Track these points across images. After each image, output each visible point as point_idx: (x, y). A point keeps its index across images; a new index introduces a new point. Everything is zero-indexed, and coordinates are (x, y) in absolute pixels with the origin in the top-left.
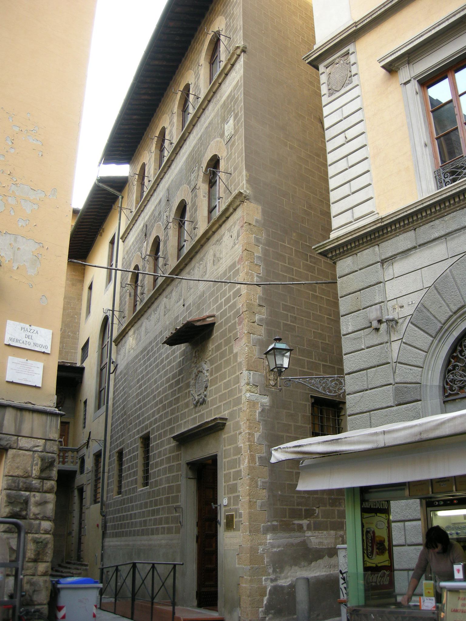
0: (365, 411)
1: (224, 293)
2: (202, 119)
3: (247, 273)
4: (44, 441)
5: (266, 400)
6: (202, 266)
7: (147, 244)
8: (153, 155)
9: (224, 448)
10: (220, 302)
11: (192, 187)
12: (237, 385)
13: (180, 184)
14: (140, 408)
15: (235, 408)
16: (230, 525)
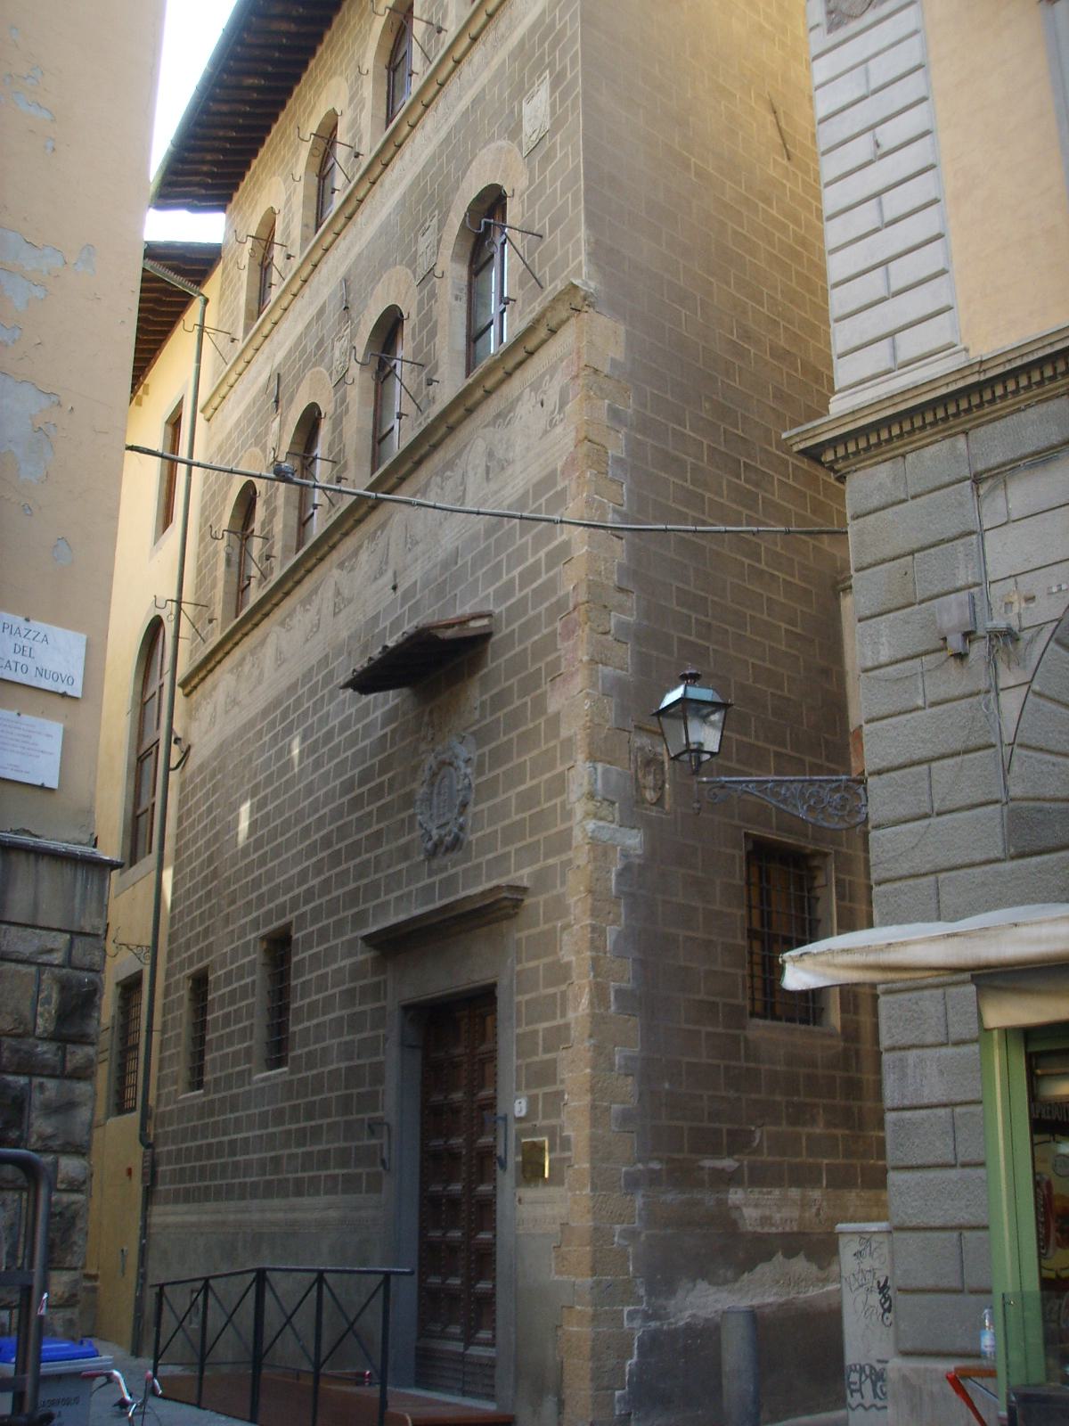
0: (923, 871)
1: (520, 556)
2: (453, 88)
3: (589, 503)
4: (68, 936)
5: (634, 840)
6: (449, 485)
7: (282, 425)
8: (300, 187)
9: (518, 968)
10: (505, 578)
11: (421, 272)
12: (558, 800)
13: (384, 265)
14: (262, 861)
15: (551, 861)
16: (531, 1171)
